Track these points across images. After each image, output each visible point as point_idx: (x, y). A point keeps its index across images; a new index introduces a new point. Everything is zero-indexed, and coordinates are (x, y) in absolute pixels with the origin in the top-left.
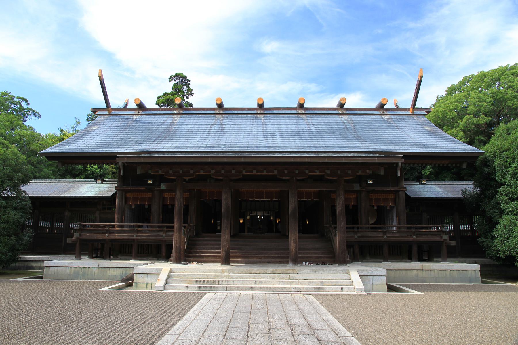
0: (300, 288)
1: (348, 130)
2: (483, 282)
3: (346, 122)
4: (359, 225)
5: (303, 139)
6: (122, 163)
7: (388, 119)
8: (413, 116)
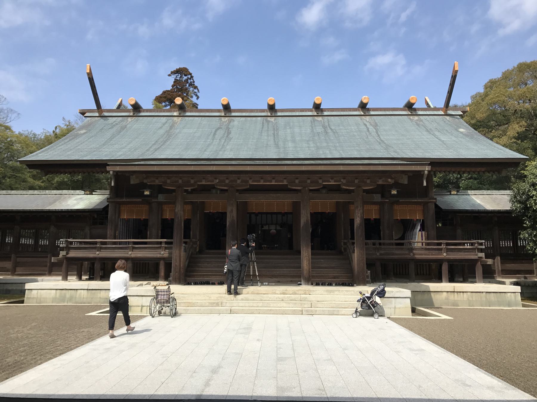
0: (312, 311)
1: (370, 134)
2: (524, 306)
3: (368, 124)
4: (382, 241)
5: (318, 144)
6: (114, 171)
7: (417, 120)
8: (446, 117)
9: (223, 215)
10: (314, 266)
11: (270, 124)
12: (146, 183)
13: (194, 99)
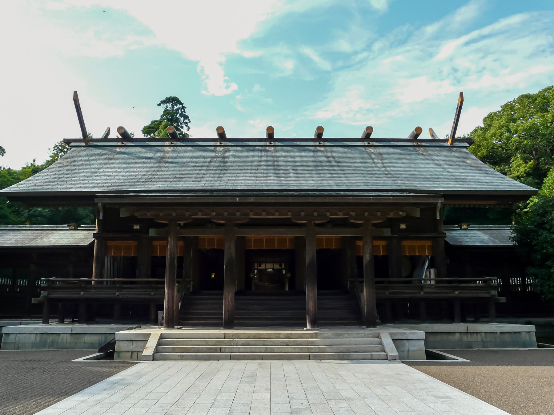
1: (376, 165)
3: (373, 155)
7: (423, 152)
9: (220, 252)
10: (319, 307)
11: (269, 153)
12: (136, 217)
13: (184, 130)
